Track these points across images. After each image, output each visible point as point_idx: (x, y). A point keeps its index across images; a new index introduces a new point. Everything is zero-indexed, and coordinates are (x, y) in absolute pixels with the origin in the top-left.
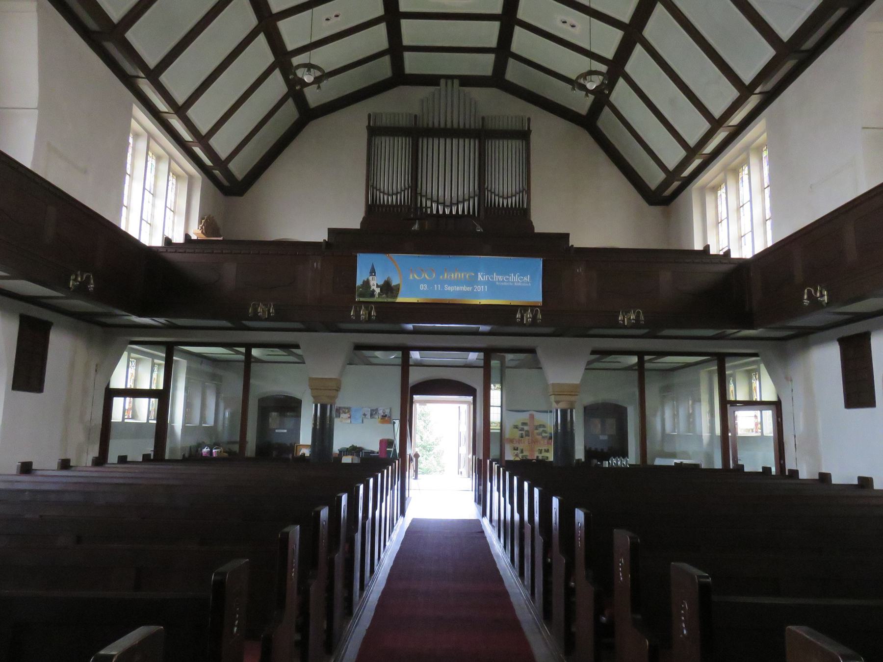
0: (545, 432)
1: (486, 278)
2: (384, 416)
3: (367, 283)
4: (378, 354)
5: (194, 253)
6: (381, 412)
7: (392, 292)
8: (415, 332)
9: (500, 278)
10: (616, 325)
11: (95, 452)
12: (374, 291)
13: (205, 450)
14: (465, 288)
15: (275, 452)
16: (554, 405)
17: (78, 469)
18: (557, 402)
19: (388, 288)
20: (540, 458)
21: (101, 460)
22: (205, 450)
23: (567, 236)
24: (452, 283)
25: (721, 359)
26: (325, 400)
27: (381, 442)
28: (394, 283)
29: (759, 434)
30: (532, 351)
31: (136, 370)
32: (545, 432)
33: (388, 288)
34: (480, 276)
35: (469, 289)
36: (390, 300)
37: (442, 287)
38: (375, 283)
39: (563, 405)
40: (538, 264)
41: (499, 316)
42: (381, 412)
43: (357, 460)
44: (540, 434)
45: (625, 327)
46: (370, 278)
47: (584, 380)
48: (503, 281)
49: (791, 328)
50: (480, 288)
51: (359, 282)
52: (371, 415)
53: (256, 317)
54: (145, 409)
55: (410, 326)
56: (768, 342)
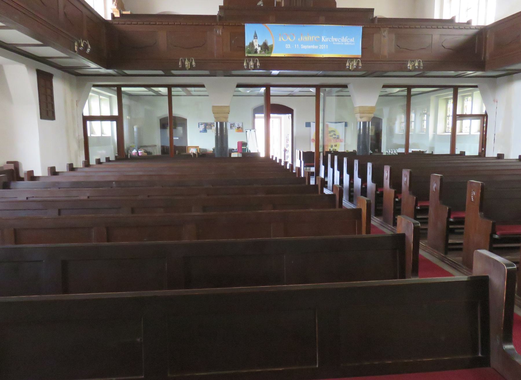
0: (335, 135)
1: (327, 40)
2: (239, 128)
3: (252, 44)
4: (192, 89)
5: (143, 24)
6: (236, 125)
7: (268, 50)
8: (278, 76)
9: (336, 39)
10: (406, 69)
11: (83, 158)
12: (256, 49)
13: (134, 151)
14: (313, 47)
15: (174, 152)
16: (359, 119)
17: (79, 170)
18: (361, 117)
19: (265, 47)
20: (331, 150)
21: (87, 164)
22: (134, 151)
23: (372, 10)
24: (305, 43)
25: (456, 89)
26: (222, 120)
27: (238, 143)
28: (269, 44)
29: (468, 134)
30: (345, 86)
31: (100, 103)
32: (335, 135)
33: (265, 47)
34: (323, 39)
35: (316, 47)
36: (267, 55)
37: (300, 46)
38: (257, 44)
39: (364, 119)
40: (359, 30)
41: (336, 65)
42: (236, 125)
43: (240, 155)
44: (331, 136)
45: (410, 71)
46: (254, 41)
47: (378, 103)
48: (338, 42)
49: (507, 70)
50: (322, 47)
51: (247, 44)
52: (231, 127)
53: (184, 68)
54: (109, 129)
55: (275, 72)
56: (482, 78)
